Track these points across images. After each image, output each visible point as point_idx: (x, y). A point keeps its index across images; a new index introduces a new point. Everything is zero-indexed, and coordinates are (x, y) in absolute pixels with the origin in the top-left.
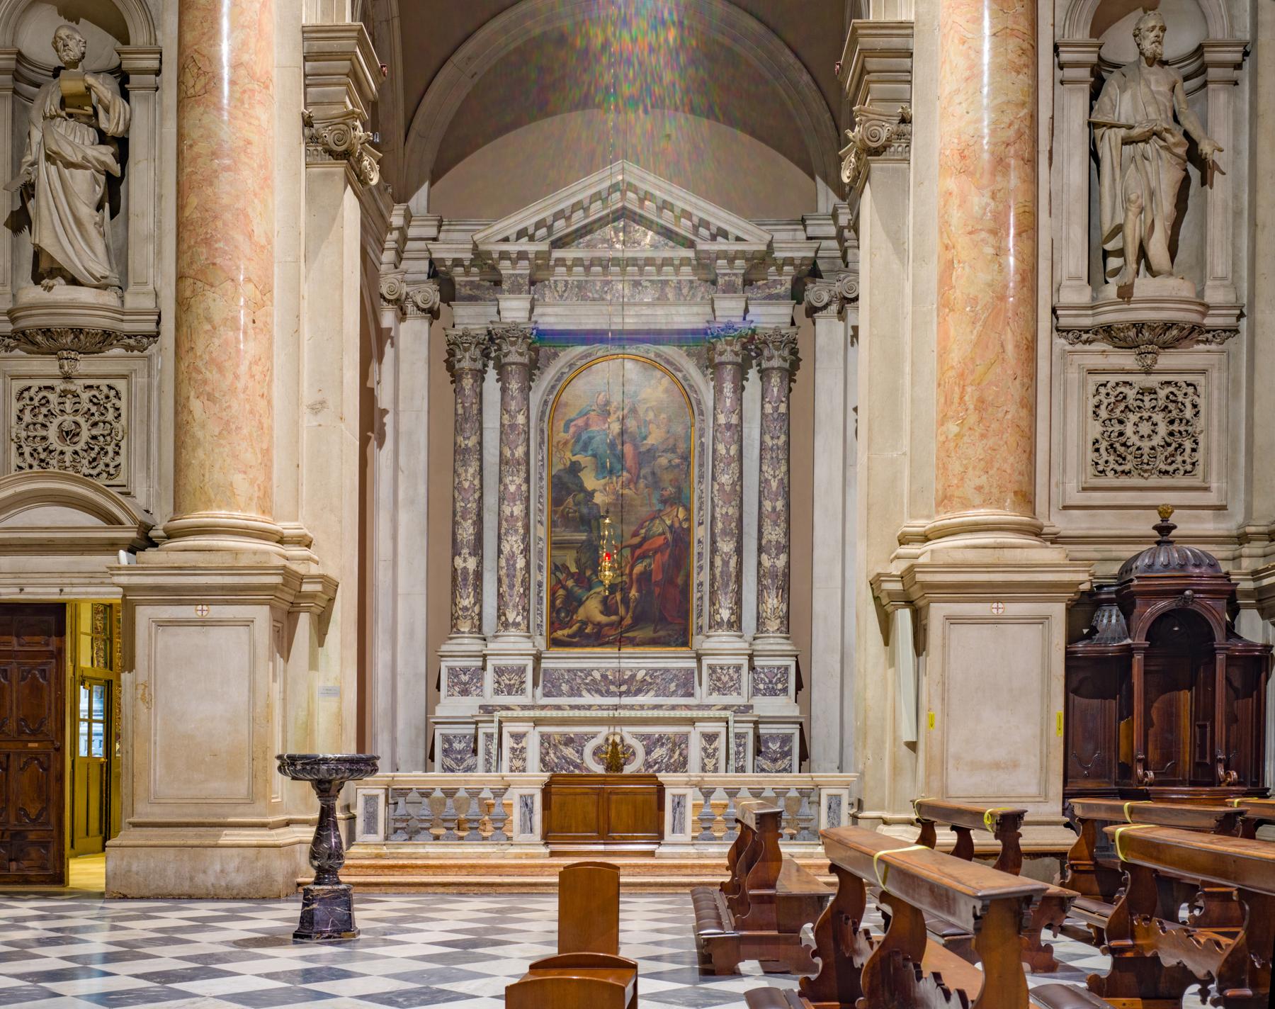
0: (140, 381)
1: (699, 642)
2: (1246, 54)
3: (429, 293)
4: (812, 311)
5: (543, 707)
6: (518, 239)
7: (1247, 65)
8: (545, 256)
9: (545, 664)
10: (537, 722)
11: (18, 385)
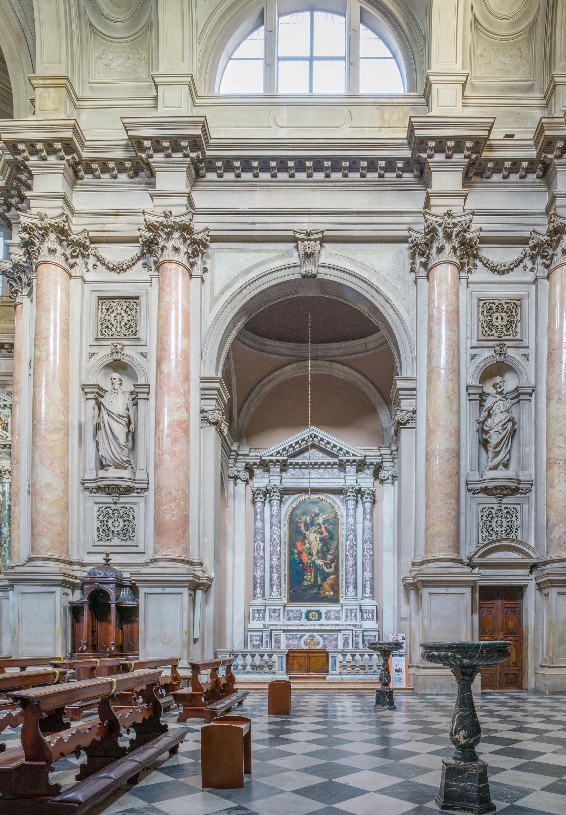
0: (142, 505)
1: (342, 601)
2: (533, 391)
3: (245, 475)
4: (382, 481)
5: (286, 625)
6: (277, 454)
7: (534, 395)
8: (284, 461)
9: (287, 608)
10: (284, 631)
11: (481, 507)
